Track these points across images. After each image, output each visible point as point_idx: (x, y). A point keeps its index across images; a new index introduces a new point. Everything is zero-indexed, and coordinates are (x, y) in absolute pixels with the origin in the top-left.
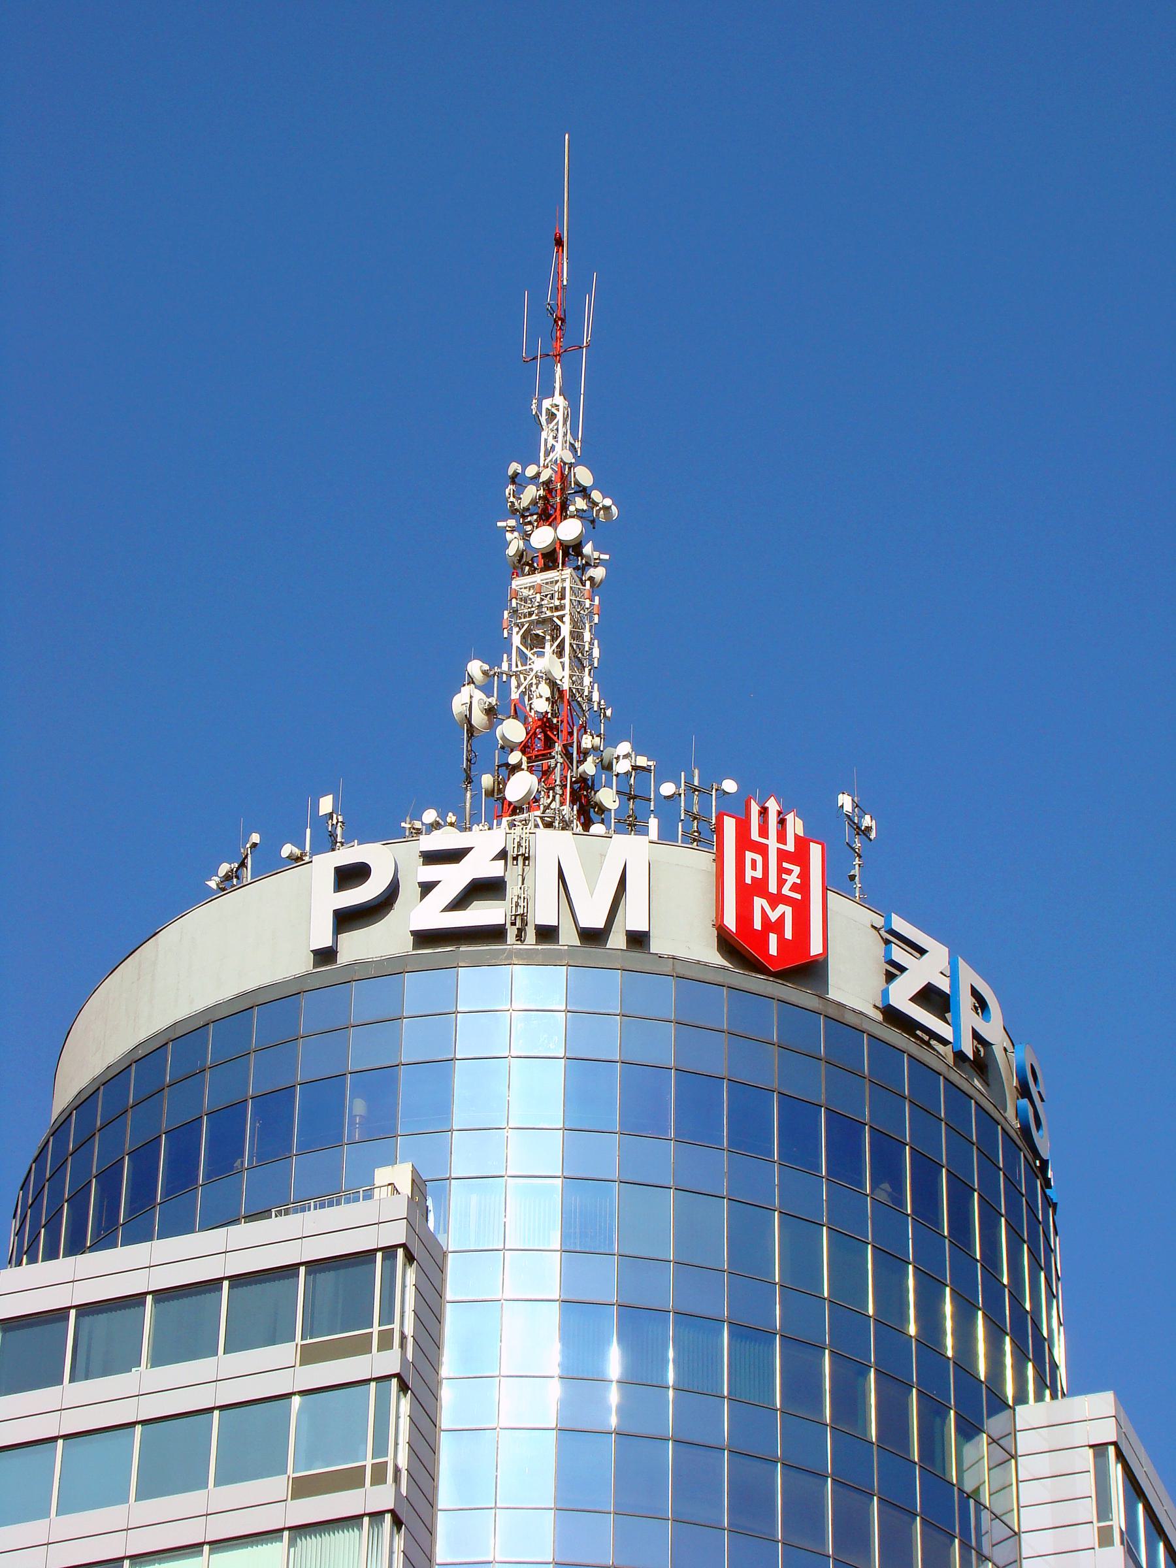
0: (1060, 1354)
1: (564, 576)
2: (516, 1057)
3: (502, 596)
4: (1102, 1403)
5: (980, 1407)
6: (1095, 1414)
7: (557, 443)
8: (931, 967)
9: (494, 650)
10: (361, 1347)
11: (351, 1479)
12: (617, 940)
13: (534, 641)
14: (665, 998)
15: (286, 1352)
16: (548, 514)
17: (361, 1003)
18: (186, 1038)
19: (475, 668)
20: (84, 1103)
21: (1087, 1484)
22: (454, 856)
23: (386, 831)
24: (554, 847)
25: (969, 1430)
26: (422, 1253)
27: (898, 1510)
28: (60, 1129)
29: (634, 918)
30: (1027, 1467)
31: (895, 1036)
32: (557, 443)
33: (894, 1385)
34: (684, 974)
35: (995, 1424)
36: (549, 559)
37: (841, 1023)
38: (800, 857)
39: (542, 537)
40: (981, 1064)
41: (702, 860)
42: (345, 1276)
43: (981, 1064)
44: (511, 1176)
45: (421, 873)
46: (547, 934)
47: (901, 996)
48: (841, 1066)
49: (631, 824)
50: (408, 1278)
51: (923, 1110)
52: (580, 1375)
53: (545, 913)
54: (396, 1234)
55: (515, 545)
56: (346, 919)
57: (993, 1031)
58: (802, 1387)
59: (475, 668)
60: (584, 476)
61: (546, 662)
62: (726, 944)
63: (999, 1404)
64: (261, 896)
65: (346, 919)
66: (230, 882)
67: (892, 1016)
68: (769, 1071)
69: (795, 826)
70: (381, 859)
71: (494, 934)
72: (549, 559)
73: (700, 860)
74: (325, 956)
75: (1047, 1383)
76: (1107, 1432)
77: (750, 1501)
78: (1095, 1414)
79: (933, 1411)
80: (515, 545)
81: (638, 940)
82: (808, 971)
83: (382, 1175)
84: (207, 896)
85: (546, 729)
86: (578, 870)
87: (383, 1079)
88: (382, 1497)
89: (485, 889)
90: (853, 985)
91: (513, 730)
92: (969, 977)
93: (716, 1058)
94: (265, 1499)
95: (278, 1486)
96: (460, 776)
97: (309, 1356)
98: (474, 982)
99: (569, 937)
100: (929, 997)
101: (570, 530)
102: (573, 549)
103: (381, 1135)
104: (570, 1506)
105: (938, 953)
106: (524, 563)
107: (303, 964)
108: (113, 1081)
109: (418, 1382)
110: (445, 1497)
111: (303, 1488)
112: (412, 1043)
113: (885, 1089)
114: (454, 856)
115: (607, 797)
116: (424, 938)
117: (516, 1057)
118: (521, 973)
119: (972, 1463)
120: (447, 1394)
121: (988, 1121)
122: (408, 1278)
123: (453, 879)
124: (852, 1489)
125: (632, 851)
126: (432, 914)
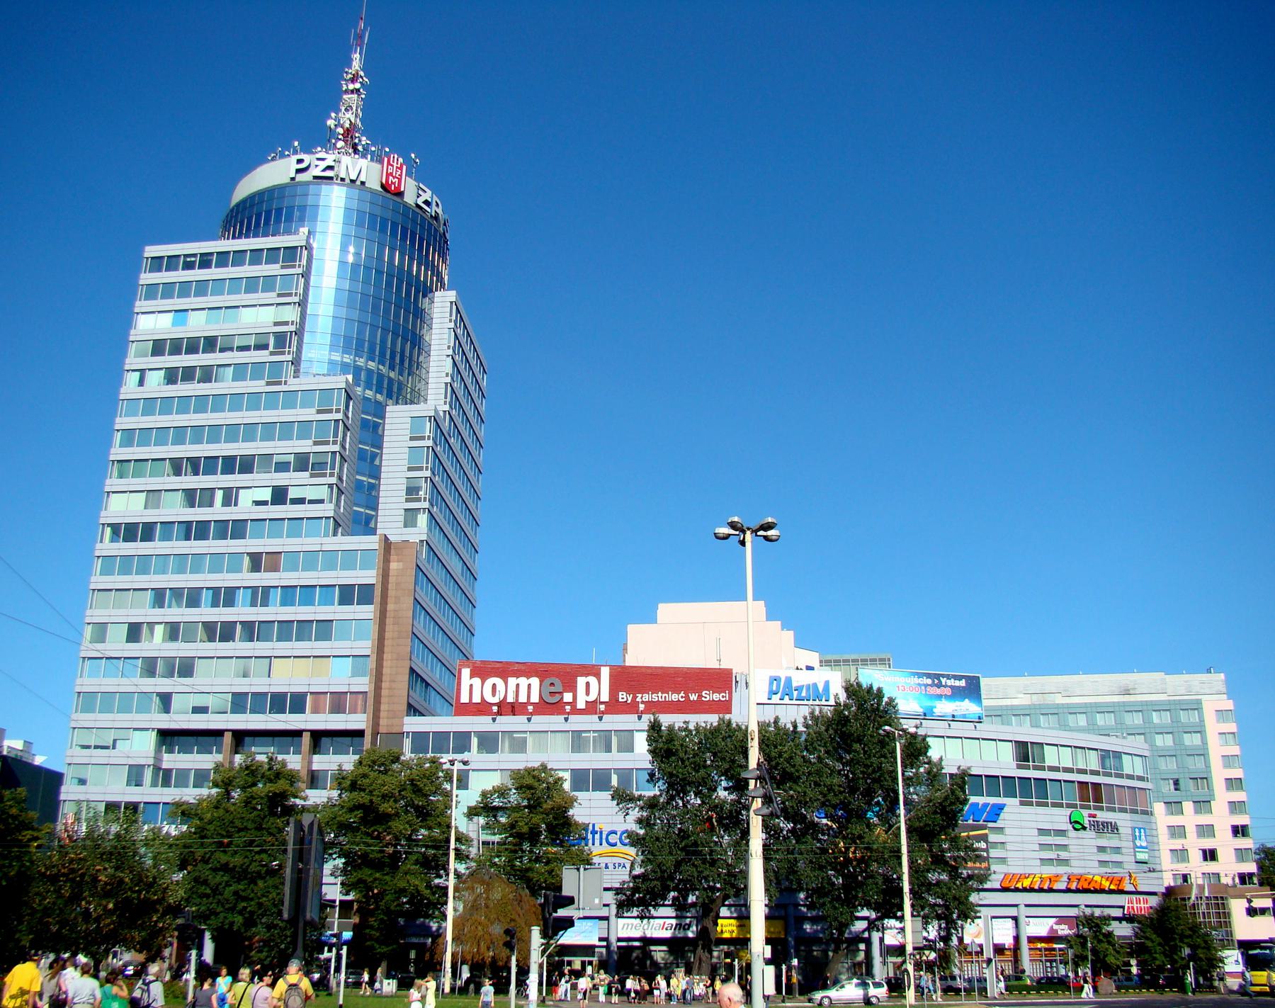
0: (446, 278)
1: (355, 96)
2: (334, 205)
3: (341, 99)
4: (454, 293)
5: (427, 291)
6: (452, 295)
7: (356, 65)
8: (427, 196)
9: (337, 111)
10: (294, 267)
11: (290, 295)
12: (358, 183)
13: (346, 110)
14: (368, 197)
15: (278, 266)
16: (353, 80)
17: (299, 190)
18: (261, 194)
19: (333, 115)
20: (238, 205)
21: (443, 391)
22: (323, 159)
23: (309, 151)
24: (346, 160)
25: (424, 296)
26: (308, 247)
27: (407, 311)
28: (232, 210)
29: (362, 178)
30: (434, 331)
31: (418, 210)
32: (356, 65)
33: (409, 285)
34: (372, 191)
35: (430, 295)
36: (352, 92)
37: (406, 206)
38: (401, 168)
39: (351, 87)
40: (436, 218)
41: (379, 166)
42: (291, 252)
43: (436, 218)
44: (331, 242)
45: (318, 161)
46: (343, 180)
47: (420, 202)
48: (405, 215)
49: (364, 156)
50: (305, 253)
51: (422, 227)
52: (344, 249)
53: (343, 175)
54: (304, 243)
55: (345, 88)
56: (298, 171)
57: (440, 211)
58: (389, 284)
59: (333, 115)
60: (362, 73)
61: (349, 115)
62: (382, 186)
63: (431, 291)
64: (280, 163)
65: (298, 171)
66: (273, 159)
67: (418, 206)
68: (389, 215)
69: (401, 160)
70: (308, 159)
71: (331, 178)
72: (352, 92)
73: (378, 166)
74: (293, 179)
75: (443, 286)
76: (454, 299)
77: (375, 307)
78: (452, 295)
79: (417, 292)
80: (345, 88)
81: (363, 183)
82: (400, 194)
83: (301, 230)
84: (268, 161)
85: (348, 131)
86: (353, 166)
87: (303, 208)
88: (296, 299)
89: (330, 168)
90: (410, 198)
91: (340, 130)
92: (435, 198)
93: (378, 211)
94: (271, 297)
95: (274, 294)
96: (324, 139)
97: (283, 267)
98: (325, 188)
99: (347, 181)
100: (426, 202)
101: (358, 86)
102: (358, 90)
103: (302, 220)
104: (346, 223)
105: (429, 192)
106: (347, 92)
107: (288, 180)
108: (244, 201)
109: (306, 275)
110: (310, 300)
111: (279, 295)
112: (310, 200)
113: (414, 221)
114: (323, 159)
115: (360, 148)
116: (315, 177)
117: (334, 205)
118: (336, 187)
119: (425, 303)
120: (309, 306)
121: (436, 230)
122: (305, 253)
123: (323, 165)
124: (398, 307)
125: (363, 163)
126: (318, 172)
